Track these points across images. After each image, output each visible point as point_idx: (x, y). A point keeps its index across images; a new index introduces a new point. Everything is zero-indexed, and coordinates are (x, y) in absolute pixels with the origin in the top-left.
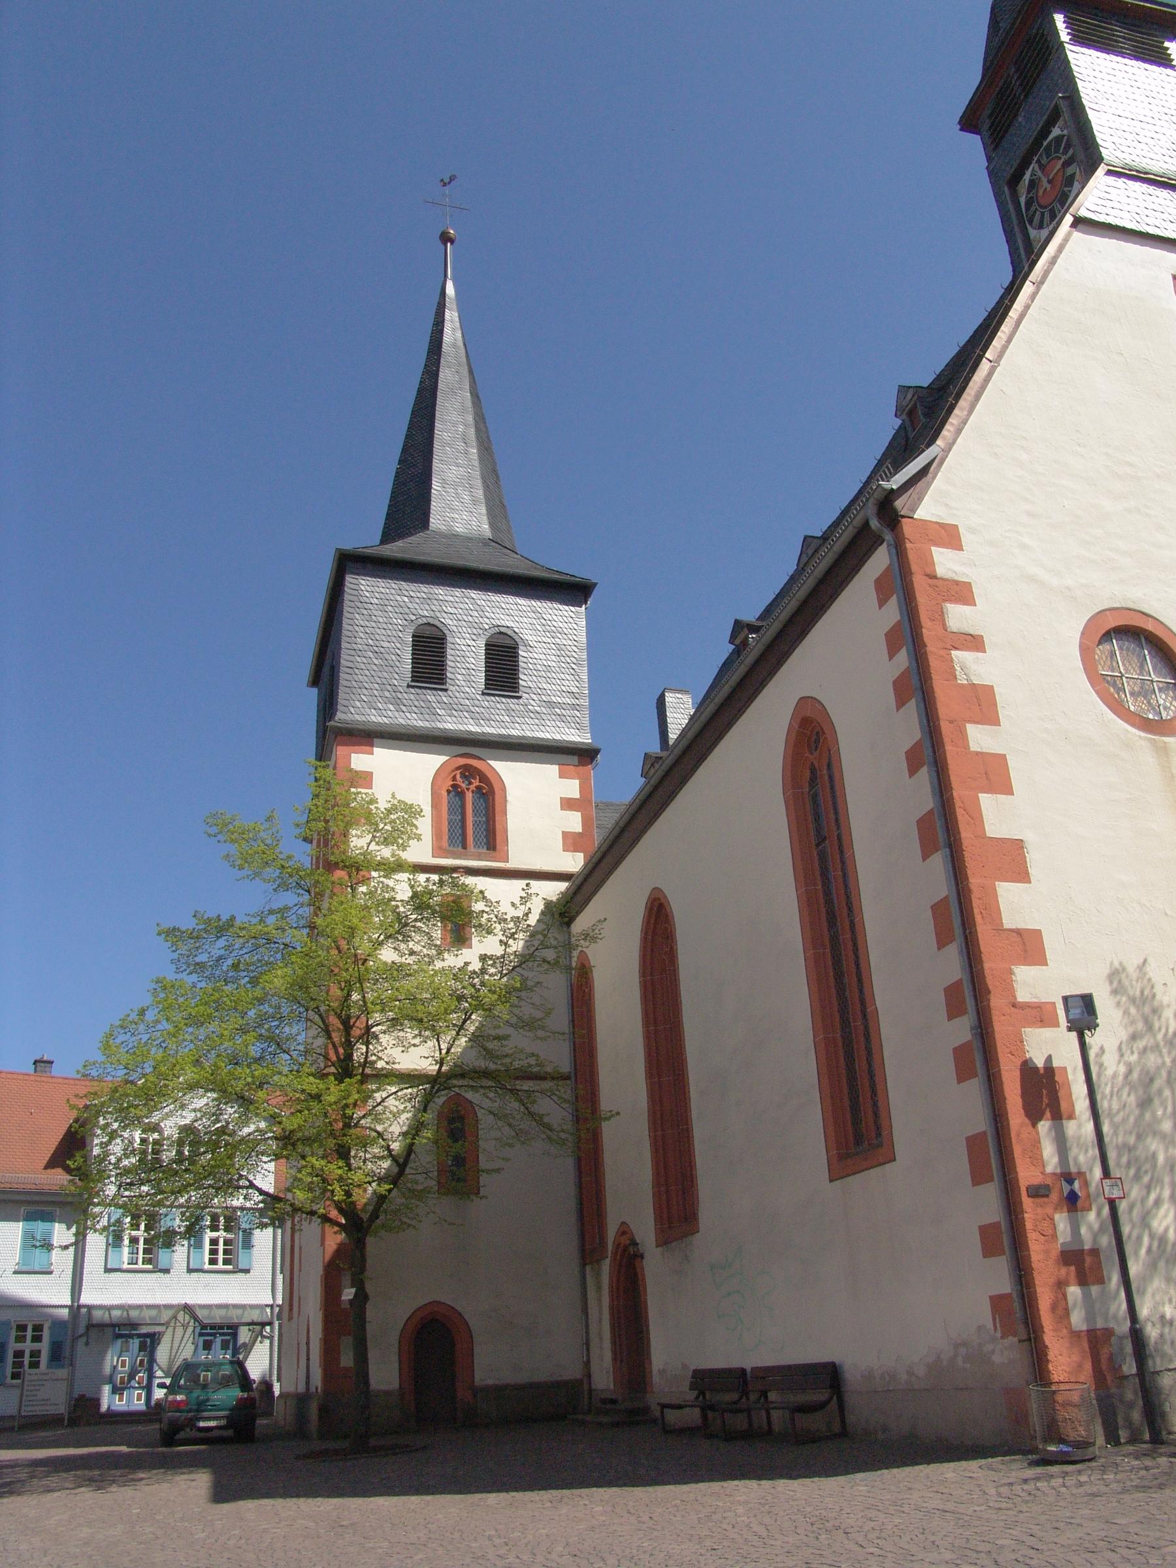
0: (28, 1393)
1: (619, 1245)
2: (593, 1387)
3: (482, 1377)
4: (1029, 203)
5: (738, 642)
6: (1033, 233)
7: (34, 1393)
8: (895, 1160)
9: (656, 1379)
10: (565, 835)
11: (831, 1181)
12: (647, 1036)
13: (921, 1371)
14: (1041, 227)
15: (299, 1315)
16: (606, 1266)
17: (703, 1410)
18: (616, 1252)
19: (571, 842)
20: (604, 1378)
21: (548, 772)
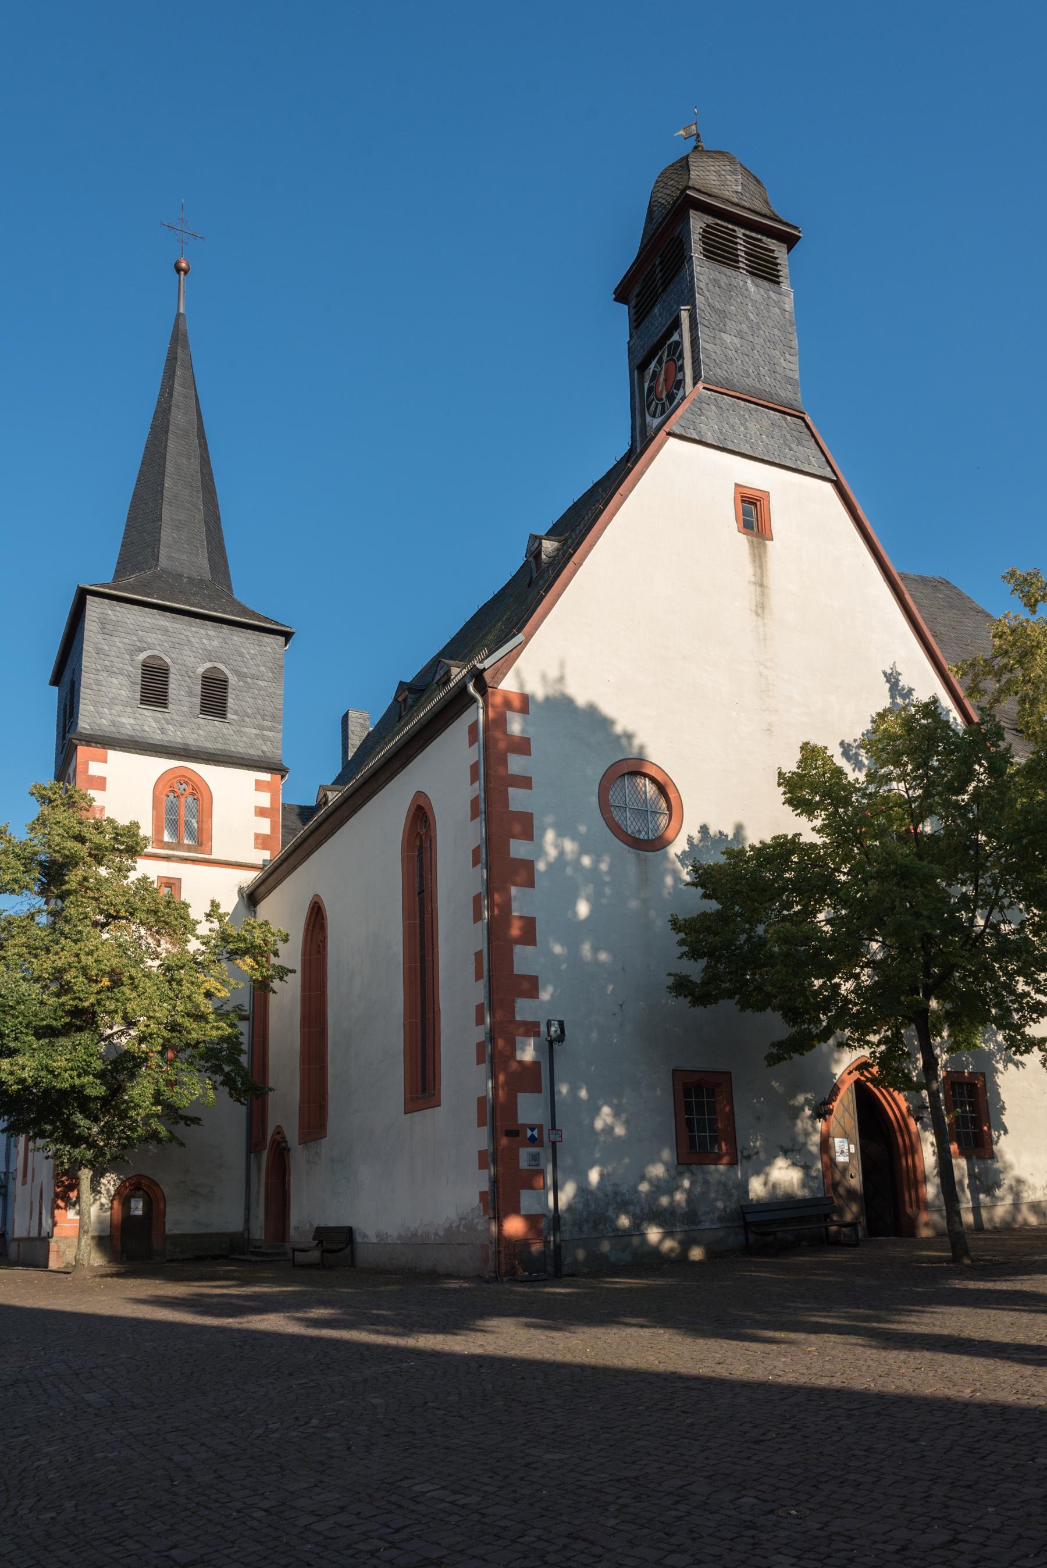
1: (275, 1140)
2: (251, 1237)
4: (650, 389)
5: (400, 699)
6: (648, 418)
8: (440, 1105)
9: (292, 1232)
10: (257, 836)
11: (405, 1113)
13: (441, 1233)
14: (654, 416)
15: (33, 1181)
16: (265, 1154)
19: (262, 842)
20: (258, 1232)
21: (249, 777)
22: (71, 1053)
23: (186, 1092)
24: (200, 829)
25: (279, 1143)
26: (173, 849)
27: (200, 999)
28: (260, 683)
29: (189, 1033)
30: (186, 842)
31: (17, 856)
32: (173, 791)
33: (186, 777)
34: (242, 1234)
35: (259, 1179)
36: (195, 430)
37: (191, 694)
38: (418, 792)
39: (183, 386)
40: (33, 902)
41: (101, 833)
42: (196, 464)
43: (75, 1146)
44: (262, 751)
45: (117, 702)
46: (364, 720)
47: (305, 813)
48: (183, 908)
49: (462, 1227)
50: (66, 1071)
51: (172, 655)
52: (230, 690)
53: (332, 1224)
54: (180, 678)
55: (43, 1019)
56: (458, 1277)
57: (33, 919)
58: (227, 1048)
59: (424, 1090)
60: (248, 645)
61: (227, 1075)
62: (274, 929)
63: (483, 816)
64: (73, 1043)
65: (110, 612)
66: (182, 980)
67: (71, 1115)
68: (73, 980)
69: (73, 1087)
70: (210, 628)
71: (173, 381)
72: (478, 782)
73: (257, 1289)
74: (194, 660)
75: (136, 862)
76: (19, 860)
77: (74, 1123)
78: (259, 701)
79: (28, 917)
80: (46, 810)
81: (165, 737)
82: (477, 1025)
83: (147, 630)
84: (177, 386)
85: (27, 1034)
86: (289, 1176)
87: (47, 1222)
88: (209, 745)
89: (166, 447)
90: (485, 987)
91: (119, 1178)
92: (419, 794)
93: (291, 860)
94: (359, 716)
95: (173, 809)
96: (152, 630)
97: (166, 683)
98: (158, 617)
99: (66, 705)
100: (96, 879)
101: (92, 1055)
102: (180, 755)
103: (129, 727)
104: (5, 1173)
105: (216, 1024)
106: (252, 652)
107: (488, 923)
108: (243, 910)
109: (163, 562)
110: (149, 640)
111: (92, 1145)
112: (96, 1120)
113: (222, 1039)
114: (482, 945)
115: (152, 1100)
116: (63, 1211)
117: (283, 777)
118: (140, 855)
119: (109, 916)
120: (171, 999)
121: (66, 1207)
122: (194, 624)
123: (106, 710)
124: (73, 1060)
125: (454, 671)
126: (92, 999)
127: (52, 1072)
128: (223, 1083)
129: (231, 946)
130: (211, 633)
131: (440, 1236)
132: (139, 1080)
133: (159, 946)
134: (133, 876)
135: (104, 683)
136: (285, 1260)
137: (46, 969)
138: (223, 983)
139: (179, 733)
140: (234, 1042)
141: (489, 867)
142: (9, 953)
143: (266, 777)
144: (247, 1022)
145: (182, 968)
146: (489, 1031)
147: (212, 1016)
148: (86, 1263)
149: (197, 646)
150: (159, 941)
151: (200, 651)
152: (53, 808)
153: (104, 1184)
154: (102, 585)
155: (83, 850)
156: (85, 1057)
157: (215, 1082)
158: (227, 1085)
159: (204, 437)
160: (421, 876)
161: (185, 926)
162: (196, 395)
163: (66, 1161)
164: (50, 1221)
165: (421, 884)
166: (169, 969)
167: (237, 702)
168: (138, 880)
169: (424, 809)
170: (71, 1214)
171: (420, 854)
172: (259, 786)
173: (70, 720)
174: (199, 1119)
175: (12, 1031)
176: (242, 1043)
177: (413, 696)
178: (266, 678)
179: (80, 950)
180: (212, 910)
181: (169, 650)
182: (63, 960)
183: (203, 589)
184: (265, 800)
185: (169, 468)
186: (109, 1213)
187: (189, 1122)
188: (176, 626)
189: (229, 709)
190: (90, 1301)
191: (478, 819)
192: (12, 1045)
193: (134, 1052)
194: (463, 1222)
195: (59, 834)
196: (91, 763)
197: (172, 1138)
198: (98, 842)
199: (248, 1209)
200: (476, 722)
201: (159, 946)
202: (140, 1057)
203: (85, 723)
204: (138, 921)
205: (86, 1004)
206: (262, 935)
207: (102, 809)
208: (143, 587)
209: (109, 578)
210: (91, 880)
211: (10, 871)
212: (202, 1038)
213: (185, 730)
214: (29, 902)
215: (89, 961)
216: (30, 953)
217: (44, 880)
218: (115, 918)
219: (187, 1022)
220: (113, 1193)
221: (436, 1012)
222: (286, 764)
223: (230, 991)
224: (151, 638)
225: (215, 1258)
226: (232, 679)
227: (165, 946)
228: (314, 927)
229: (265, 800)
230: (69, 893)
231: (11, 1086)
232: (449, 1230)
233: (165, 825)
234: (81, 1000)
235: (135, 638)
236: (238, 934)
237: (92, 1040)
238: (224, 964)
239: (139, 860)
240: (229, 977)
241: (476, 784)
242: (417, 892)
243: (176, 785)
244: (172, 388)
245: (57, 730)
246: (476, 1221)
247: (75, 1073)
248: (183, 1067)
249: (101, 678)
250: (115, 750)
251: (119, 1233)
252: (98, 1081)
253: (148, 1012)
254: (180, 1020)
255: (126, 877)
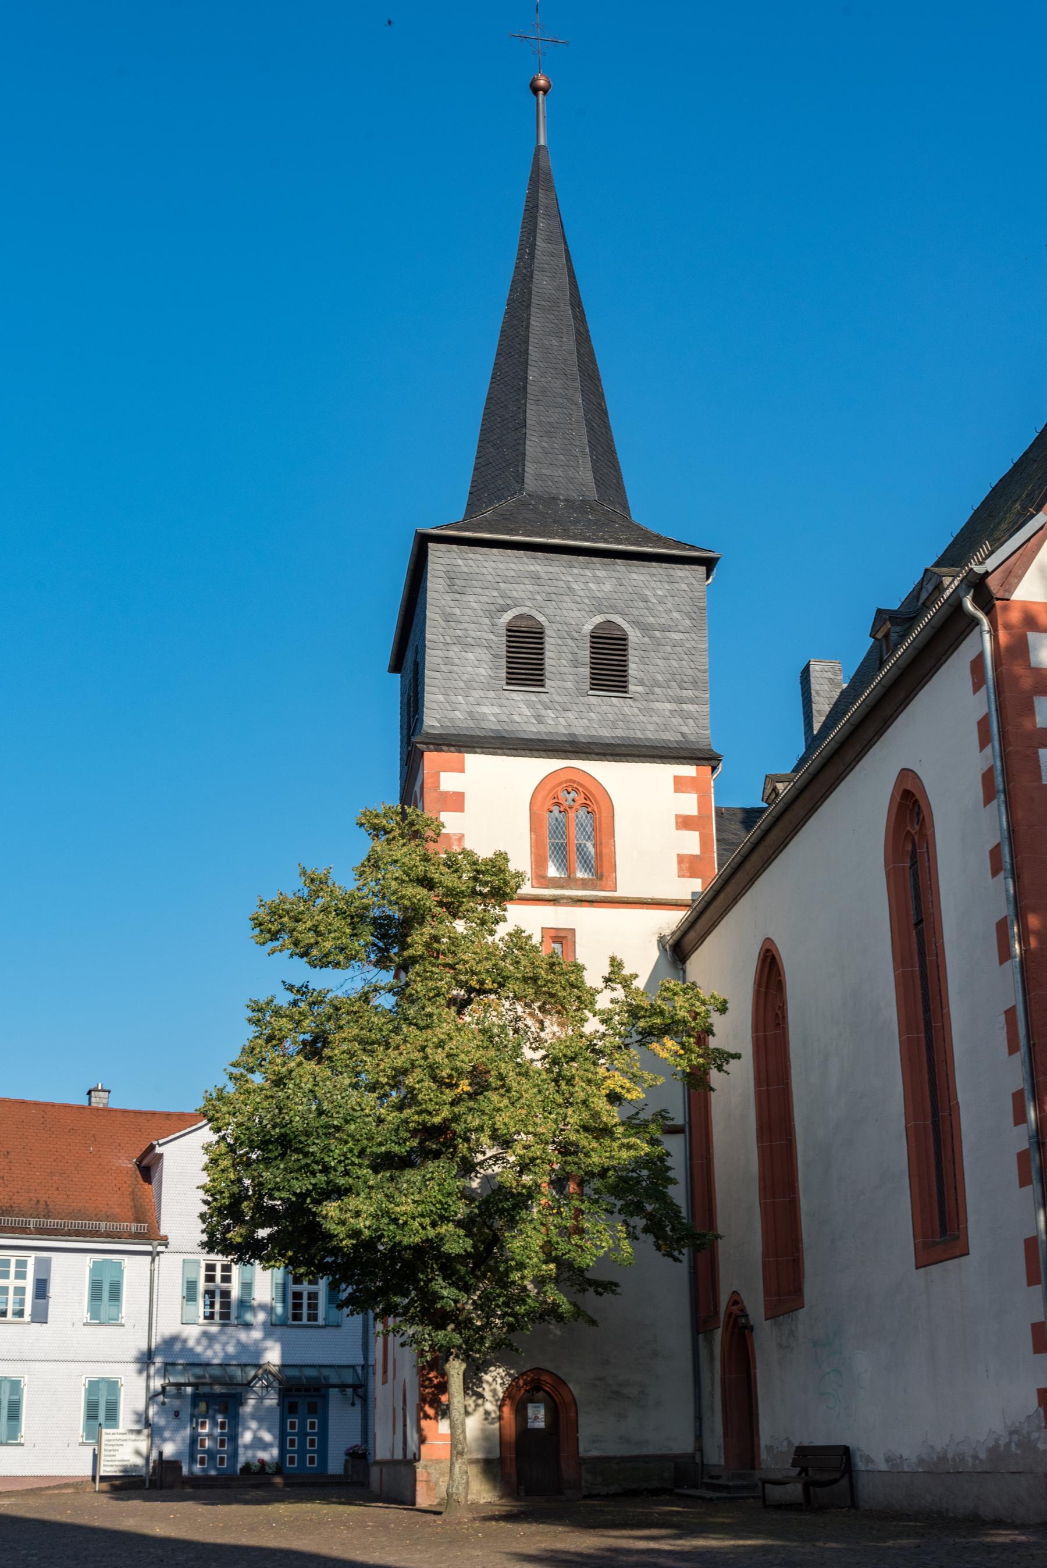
0: (107, 1453)
2: (705, 1462)
3: (587, 1448)
5: (879, 636)
7: (112, 1453)
8: (968, 1254)
9: (764, 1455)
10: (681, 858)
12: (759, 1095)
13: (983, 1455)
16: (718, 1334)
17: (806, 1486)
18: (728, 1321)
20: (715, 1455)
21: (667, 772)
22: (419, 1193)
23: (588, 1245)
24: (599, 856)
25: (737, 1317)
26: (562, 887)
27: (601, 1104)
28: (676, 636)
29: (587, 1155)
30: (580, 875)
31: (340, 912)
32: (558, 804)
33: (574, 781)
34: (692, 1456)
35: (712, 1373)
36: (568, 297)
37: (576, 663)
38: (903, 770)
39: (548, 241)
40: (369, 976)
41: (456, 871)
42: (570, 343)
43: (441, 1326)
44: (682, 734)
45: (475, 685)
46: (835, 674)
47: (750, 816)
48: (572, 972)
49: (1013, 1445)
50: (414, 1218)
51: (547, 611)
52: (630, 651)
53: (820, 1441)
54: (560, 641)
55: (380, 1144)
56: (1013, 1526)
57: (367, 1001)
58: (649, 1177)
59: (944, 1231)
60: (653, 584)
61: (650, 1216)
62: (704, 994)
63: (1002, 797)
64: (424, 1176)
65: (460, 562)
66: (573, 1077)
67: (431, 1280)
68: (417, 1086)
69: (427, 1240)
70: (599, 566)
71: (535, 237)
72: (989, 747)
73: (700, 1542)
74: (579, 614)
75: (505, 910)
76: (345, 918)
77: (435, 1293)
78: (674, 662)
79: (360, 999)
80: (380, 845)
81: (542, 728)
82: (1016, 1124)
83: (511, 580)
84: (539, 242)
85: (360, 1166)
86: (755, 1368)
87: (412, 1436)
88: (606, 733)
89: (528, 327)
90: (1023, 1063)
91: (508, 1374)
92: (906, 773)
93: (730, 889)
94: (826, 668)
95: (559, 830)
96: (518, 580)
97: (540, 652)
98: (525, 559)
99: (409, 696)
100: (450, 938)
101: (449, 1195)
102: (566, 752)
103: (492, 718)
104: (363, 1366)
105: (626, 1141)
106: (660, 592)
107: (1021, 961)
108: (666, 968)
109: (531, 483)
110: (515, 594)
111: (463, 1324)
112: (467, 1289)
113: (641, 1163)
114: (1014, 997)
115: (542, 1256)
116: (433, 1422)
117: (714, 769)
118: (511, 899)
119: (470, 990)
120: (560, 1105)
121: (437, 1414)
122: (575, 564)
123: (460, 698)
124: (423, 1202)
125: (947, 581)
126: (445, 1113)
127: (395, 1221)
128: (646, 1230)
129: (642, 1024)
130: (601, 573)
131: (981, 1461)
132: (520, 1226)
133: (542, 1030)
134: (503, 930)
135: (457, 661)
136: (753, 1497)
137: (384, 1071)
138: (634, 1078)
139: (561, 720)
140: (657, 1166)
141: (1016, 876)
142: (336, 1052)
143: (689, 771)
144: (682, 1136)
145: (573, 1059)
146: (1034, 1133)
147: (620, 1129)
148: (462, 1499)
149: (581, 593)
150: (541, 1022)
151: (587, 601)
152: (389, 842)
153: (488, 1382)
154: (449, 527)
155: (429, 899)
156: (440, 1197)
157: (634, 1227)
158: (651, 1232)
159: (579, 305)
160: (917, 897)
161: (579, 998)
162: (567, 251)
163: (427, 1348)
164: (416, 1436)
165: (918, 910)
166: (555, 1062)
167: (641, 667)
168: (510, 935)
169: (913, 795)
170: (443, 1427)
171: (914, 864)
172: (680, 784)
173: (414, 716)
174: (616, 1285)
175: (340, 1162)
176: (669, 1169)
177: (898, 629)
178: (681, 628)
179: (426, 1041)
180: (612, 972)
181: (543, 604)
182: (403, 1058)
183: (587, 513)
184: (689, 804)
185: (534, 353)
186: (497, 1425)
187: (600, 1290)
188: (551, 569)
189: (630, 679)
190: (457, 1557)
191: (995, 802)
192: (341, 1181)
193: (511, 1187)
194: (1015, 1438)
195: (396, 879)
196: (443, 775)
197: (578, 1312)
198: (450, 885)
199: (699, 1418)
200: (981, 655)
201: (542, 1030)
202: (520, 1194)
203: (432, 720)
204: (511, 995)
205: (437, 1120)
206: (686, 1005)
207: (461, 838)
208: (503, 522)
209: (458, 514)
210: (445, 940)
211: (332, 935)
212: (607, 1163)
213: (570, 714)
214: (363, 976)
215: (439, 1056)
216: (364, 1050)
217: (381, 944)
218: (481, 992)
219: (585, 1141)
220: (501, 1395)
221: (954, 1109)
222: (717, 749)
223: (644, 1091)
224: (517, 591)
225: (655, 1492)
226: (634, 636)
227: (552, 1030)
228: (767, 988)
229: (689, 804)
230: (414, 960)
231: (341, 1241)
232: (993, 1450)
233: (549, 853)
234: (430, 1113)
235: (495, 594)
236: (652, 1005)
237: (449, 1172)
238: (634, 1051)
239: (510, 907)
240: (641, 1069)
241: (988, 749)
242: (913, 922)
243: (563, 795)
244: (533, 246)
245: (401, 734)
246: (1035, 1435)
247: (427, 1221)
248: (583, 1207)
249: (452, 654)
250: (476, 753)
251: (513, 1456)
252: (462, 1232)
253: (526, 1126)
254: (573, 1137)
255: (492, 933)
